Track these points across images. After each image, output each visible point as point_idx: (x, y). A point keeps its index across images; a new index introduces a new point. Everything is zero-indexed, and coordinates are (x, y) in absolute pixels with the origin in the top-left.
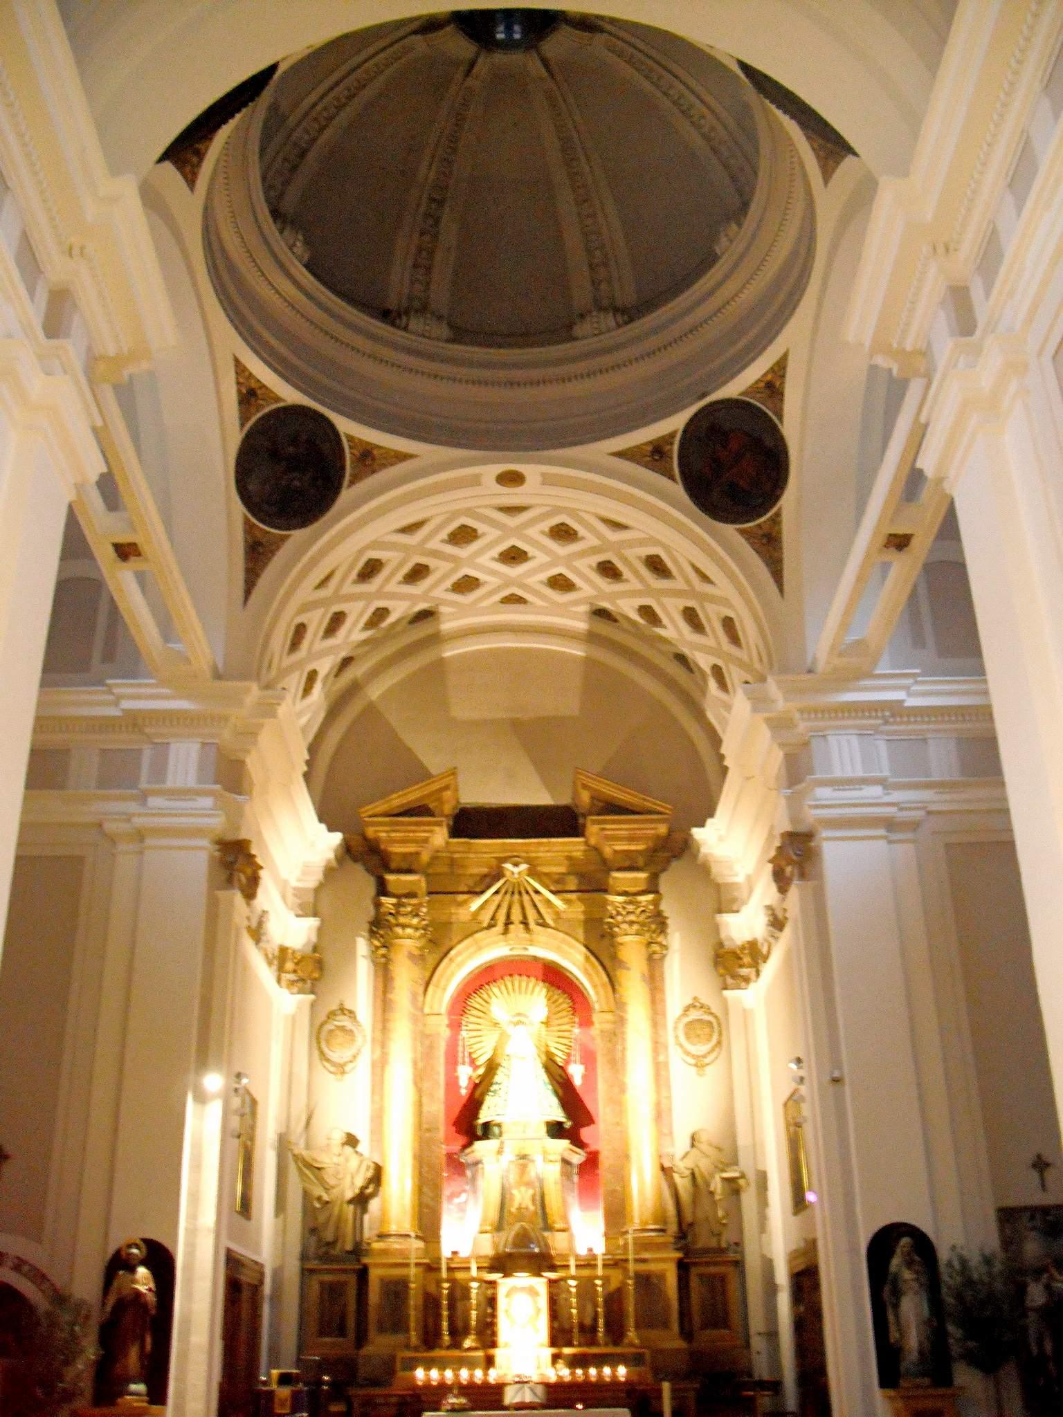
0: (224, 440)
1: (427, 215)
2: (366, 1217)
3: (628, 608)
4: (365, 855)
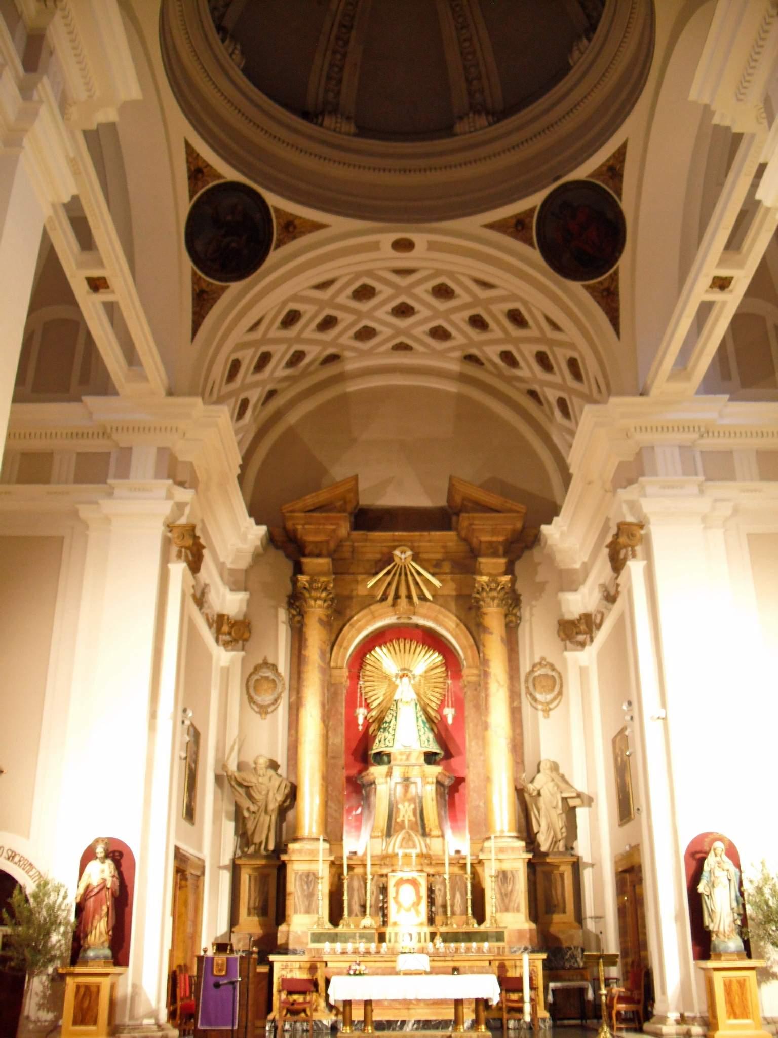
0: (176, 204)
1: (338, 38)
2: (284, 825)
3: (492, 353)
4: (286, 544)
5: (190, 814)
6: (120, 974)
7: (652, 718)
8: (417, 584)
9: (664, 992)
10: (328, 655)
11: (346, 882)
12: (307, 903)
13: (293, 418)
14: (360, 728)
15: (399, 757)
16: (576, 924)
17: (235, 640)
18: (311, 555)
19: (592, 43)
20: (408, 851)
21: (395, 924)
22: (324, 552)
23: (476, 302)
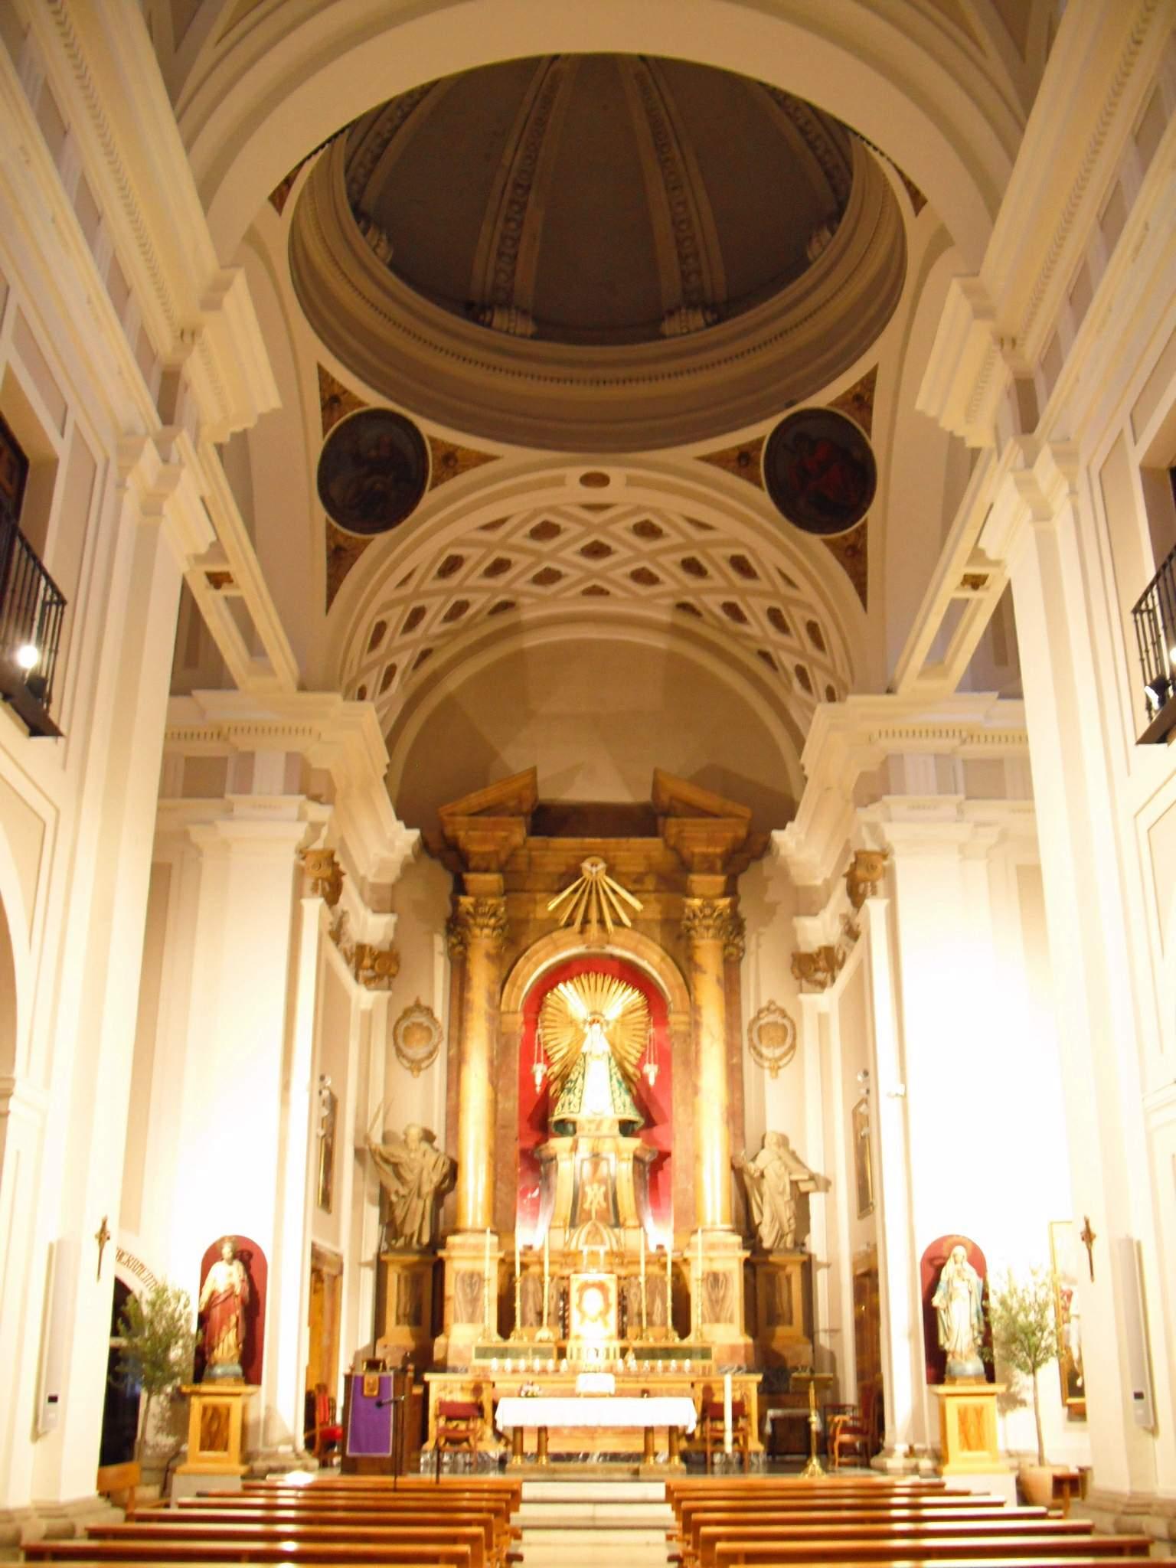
1: (512, 202)
2: (442, 1211)
3: (713, 603)
4: (444, 853)
5: (326, 1200)
6: (251, 1395)
7: (889, 1095)
8: (611, 905)
9: (893, 1422)
10: (497, 997)
11: (518, 1285)
12: (470, 1310)
13: (452, 683)
14: (538, 1089)
15: (587, 1127)
16: (804, 1339)
17: (378, 977)
18: (477, 870)
19: (837, 236)
20: (595, 1248)
21: (578, 1337)
22: (494, 866)
23: (690, 543)
